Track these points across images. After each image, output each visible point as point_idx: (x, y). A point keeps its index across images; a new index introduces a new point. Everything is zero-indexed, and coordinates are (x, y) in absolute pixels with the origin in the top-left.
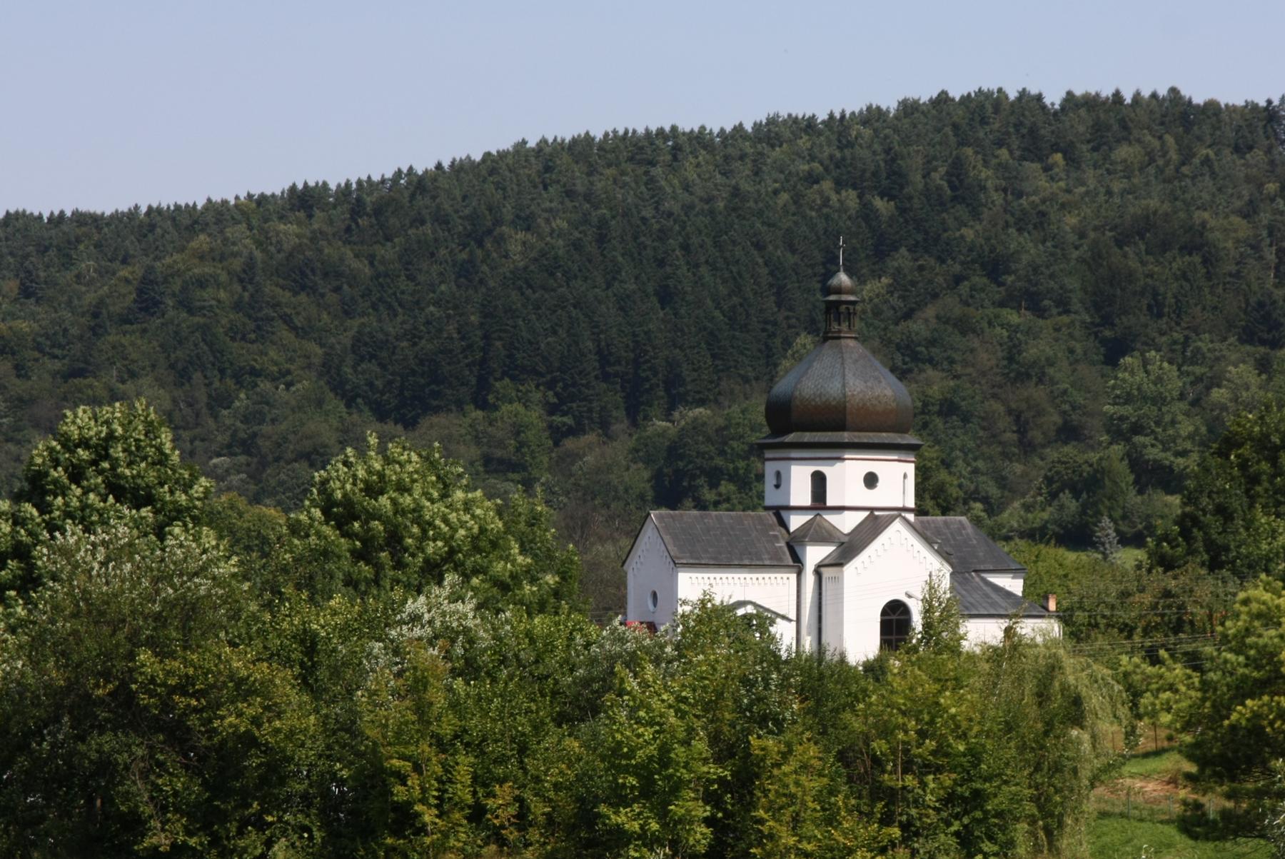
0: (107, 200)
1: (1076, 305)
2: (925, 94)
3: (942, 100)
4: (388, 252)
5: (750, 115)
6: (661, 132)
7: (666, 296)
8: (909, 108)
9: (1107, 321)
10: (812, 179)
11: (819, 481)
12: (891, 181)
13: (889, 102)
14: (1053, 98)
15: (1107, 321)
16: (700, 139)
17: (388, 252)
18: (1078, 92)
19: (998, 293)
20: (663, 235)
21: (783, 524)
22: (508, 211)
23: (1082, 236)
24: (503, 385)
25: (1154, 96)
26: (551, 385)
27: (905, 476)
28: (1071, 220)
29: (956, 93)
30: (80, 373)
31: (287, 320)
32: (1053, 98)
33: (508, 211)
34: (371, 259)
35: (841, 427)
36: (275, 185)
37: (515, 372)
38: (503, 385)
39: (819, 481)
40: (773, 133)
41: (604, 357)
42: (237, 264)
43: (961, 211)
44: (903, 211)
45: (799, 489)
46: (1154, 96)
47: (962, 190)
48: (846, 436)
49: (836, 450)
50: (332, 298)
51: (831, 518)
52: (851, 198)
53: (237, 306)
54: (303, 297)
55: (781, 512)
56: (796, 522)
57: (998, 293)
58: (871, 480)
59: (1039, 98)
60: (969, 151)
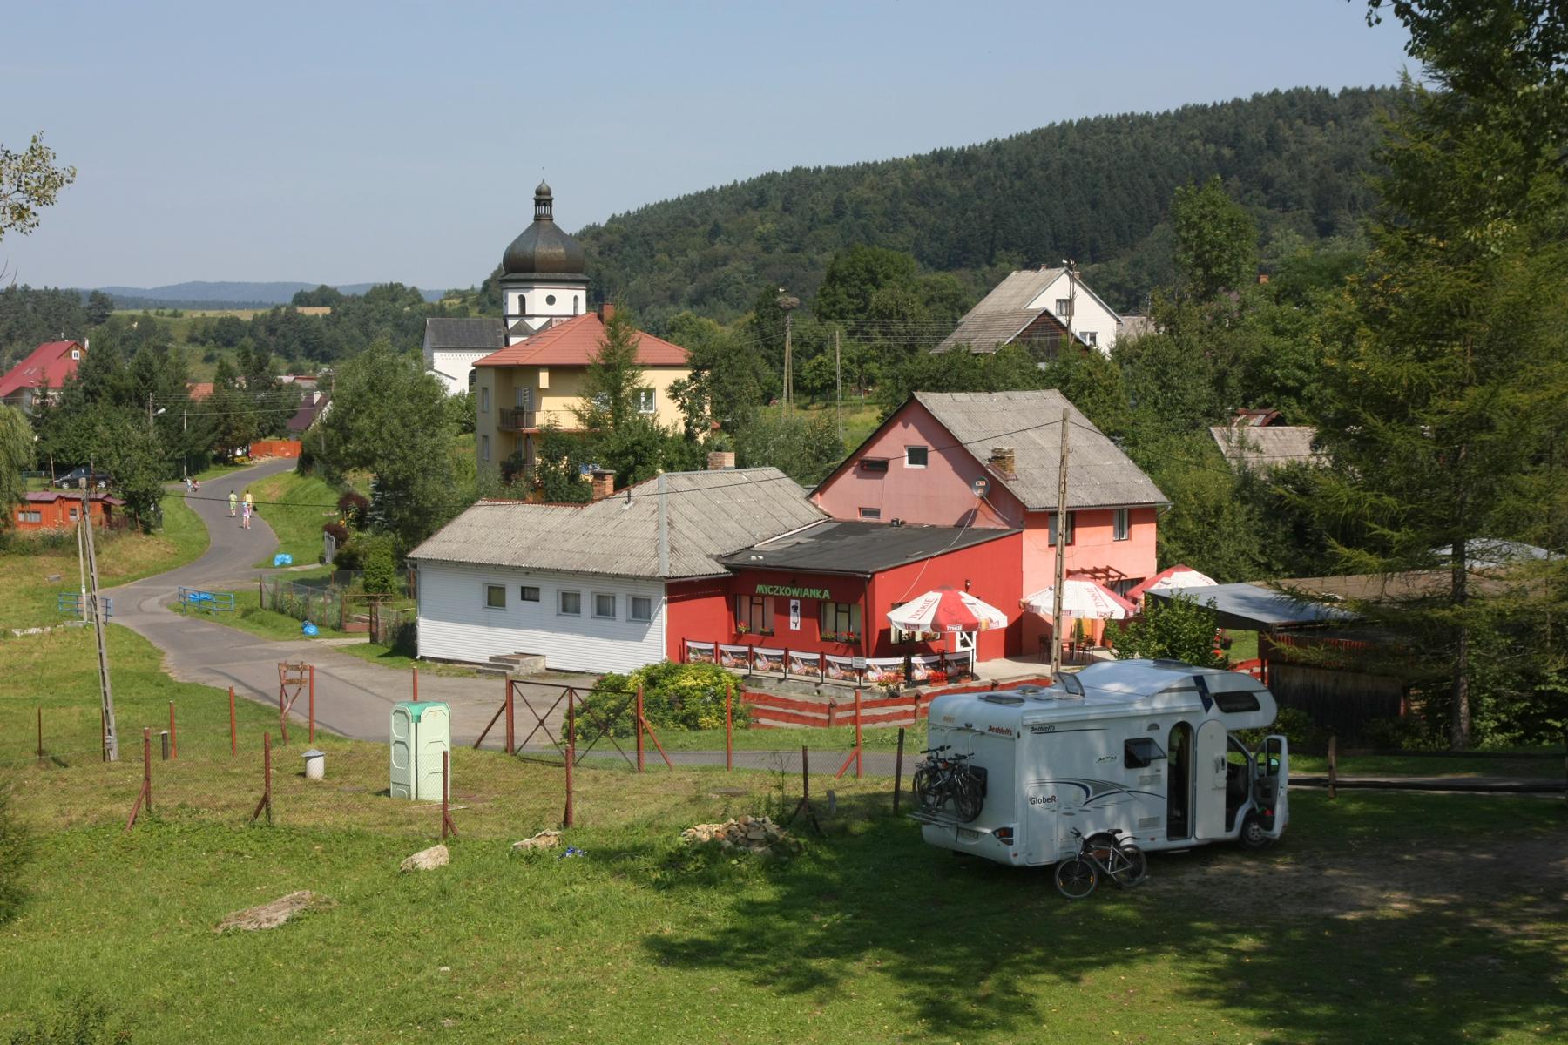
0: (841, 162)
1: (1307, 203)
2: (1265, 90)
3: (1276, 93)
4: (968, 184)
5: (1173, 106)
6: (1125, 116)
7: (1094, 205)
8: (1257, 98)
9: (1325, 212)
10: (1192, 138)
11: (522, 300)
12: (1235, 141)
13: (1246, 96)
14: (1335, 91)
15: (1325, 212)
16: (1145, 119)
17: (968, 184)
18: (1350, 87)
19: (1265, 198)
20: (1098, 170)
21: (506, 324)
22: (1037, 161)
23: (1316, 166)
24: (1000, 253)
25: (1393, 88)
26: (1026, 253)
27: (576, 298)
28: (1312, 159)
29: (1283, 90)
30: (795, 250)
31: (911, 221)
32: (1335, 91)
33: (1037, 161)
34: (960, 187)
35: (533, 270)
36: (925, 150)
37: (1007, 246)
38: (1000, 253)
39: (522, 300)
40: (1187, 115)
41: (1056, 237)
42: (889, 192)
43: (1271, 154)
44: (1238, 155)
45: (513, 307)
46: (1393, 88)
47: (1273, 143)
48: (535, 275)
49: (529, 283)
50: (937, 208)
51: (528, 321)
52: (1211, 148)
53: (884, 214)
54: (922, 208)
55: (506, 318)
56: (512, 323)
57: (1265, 198)
58: (551, 300)
59: (1326, 91)
60: (1280, 121)
